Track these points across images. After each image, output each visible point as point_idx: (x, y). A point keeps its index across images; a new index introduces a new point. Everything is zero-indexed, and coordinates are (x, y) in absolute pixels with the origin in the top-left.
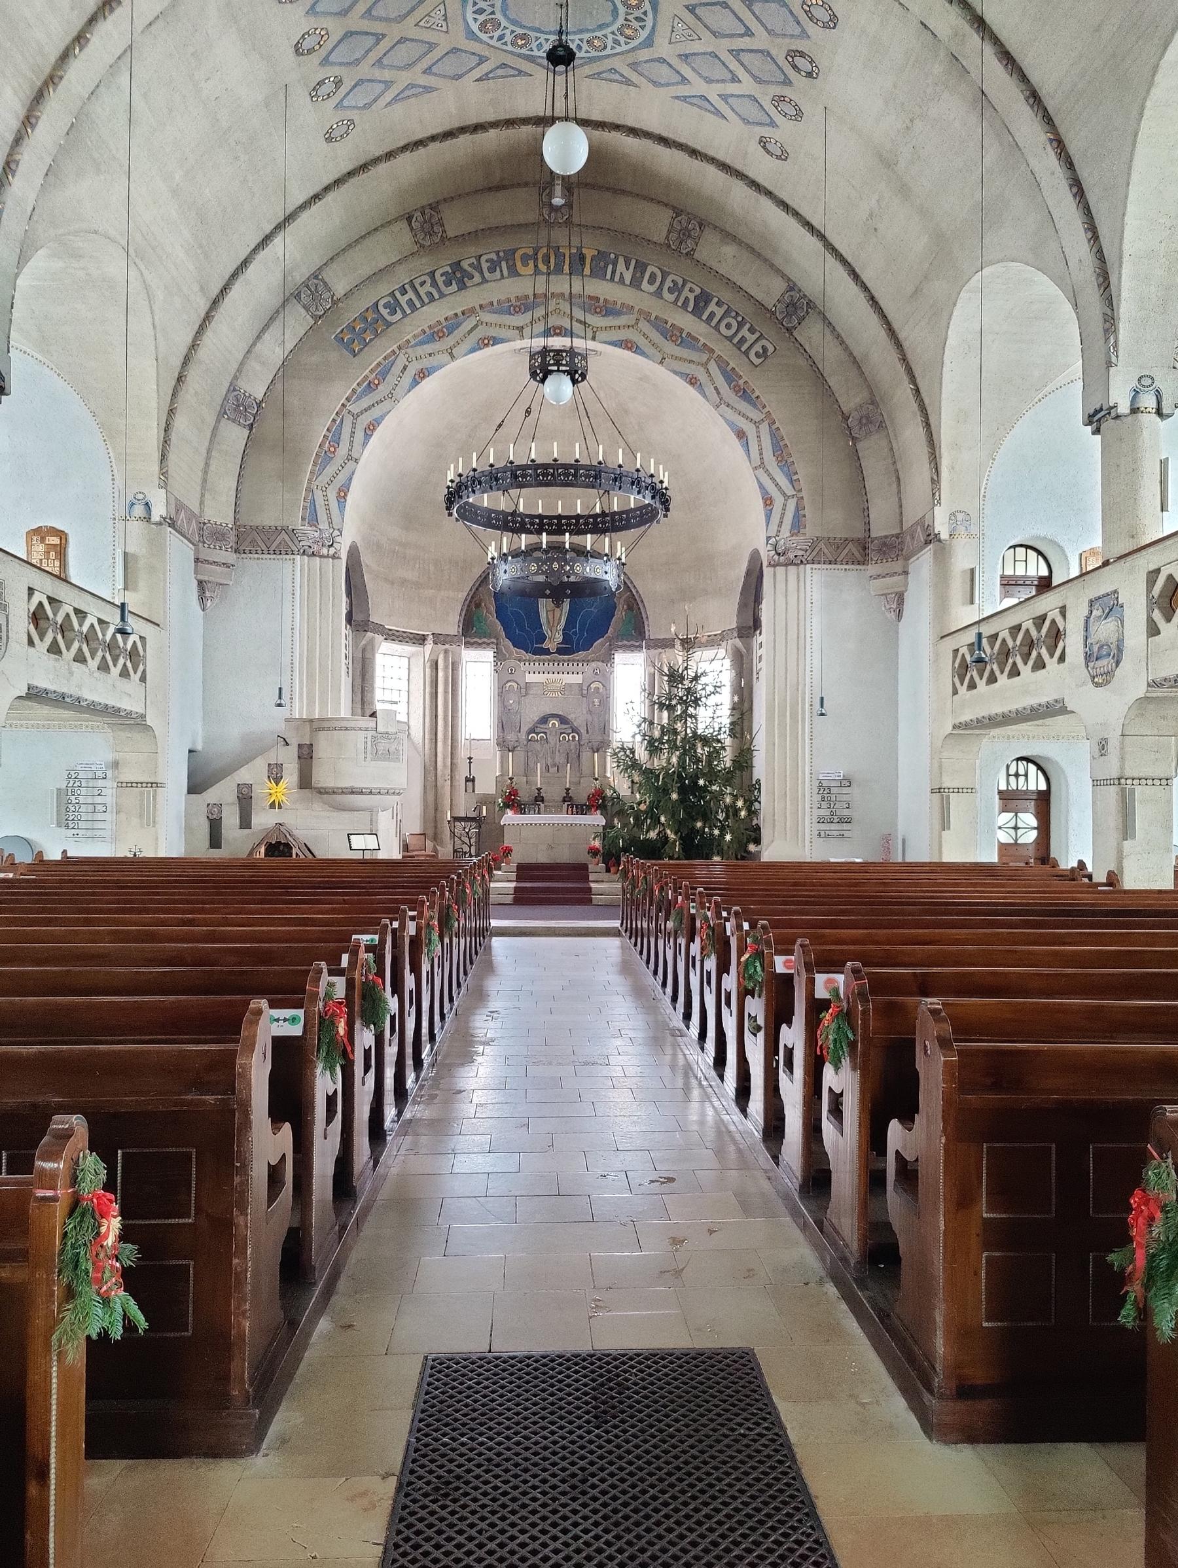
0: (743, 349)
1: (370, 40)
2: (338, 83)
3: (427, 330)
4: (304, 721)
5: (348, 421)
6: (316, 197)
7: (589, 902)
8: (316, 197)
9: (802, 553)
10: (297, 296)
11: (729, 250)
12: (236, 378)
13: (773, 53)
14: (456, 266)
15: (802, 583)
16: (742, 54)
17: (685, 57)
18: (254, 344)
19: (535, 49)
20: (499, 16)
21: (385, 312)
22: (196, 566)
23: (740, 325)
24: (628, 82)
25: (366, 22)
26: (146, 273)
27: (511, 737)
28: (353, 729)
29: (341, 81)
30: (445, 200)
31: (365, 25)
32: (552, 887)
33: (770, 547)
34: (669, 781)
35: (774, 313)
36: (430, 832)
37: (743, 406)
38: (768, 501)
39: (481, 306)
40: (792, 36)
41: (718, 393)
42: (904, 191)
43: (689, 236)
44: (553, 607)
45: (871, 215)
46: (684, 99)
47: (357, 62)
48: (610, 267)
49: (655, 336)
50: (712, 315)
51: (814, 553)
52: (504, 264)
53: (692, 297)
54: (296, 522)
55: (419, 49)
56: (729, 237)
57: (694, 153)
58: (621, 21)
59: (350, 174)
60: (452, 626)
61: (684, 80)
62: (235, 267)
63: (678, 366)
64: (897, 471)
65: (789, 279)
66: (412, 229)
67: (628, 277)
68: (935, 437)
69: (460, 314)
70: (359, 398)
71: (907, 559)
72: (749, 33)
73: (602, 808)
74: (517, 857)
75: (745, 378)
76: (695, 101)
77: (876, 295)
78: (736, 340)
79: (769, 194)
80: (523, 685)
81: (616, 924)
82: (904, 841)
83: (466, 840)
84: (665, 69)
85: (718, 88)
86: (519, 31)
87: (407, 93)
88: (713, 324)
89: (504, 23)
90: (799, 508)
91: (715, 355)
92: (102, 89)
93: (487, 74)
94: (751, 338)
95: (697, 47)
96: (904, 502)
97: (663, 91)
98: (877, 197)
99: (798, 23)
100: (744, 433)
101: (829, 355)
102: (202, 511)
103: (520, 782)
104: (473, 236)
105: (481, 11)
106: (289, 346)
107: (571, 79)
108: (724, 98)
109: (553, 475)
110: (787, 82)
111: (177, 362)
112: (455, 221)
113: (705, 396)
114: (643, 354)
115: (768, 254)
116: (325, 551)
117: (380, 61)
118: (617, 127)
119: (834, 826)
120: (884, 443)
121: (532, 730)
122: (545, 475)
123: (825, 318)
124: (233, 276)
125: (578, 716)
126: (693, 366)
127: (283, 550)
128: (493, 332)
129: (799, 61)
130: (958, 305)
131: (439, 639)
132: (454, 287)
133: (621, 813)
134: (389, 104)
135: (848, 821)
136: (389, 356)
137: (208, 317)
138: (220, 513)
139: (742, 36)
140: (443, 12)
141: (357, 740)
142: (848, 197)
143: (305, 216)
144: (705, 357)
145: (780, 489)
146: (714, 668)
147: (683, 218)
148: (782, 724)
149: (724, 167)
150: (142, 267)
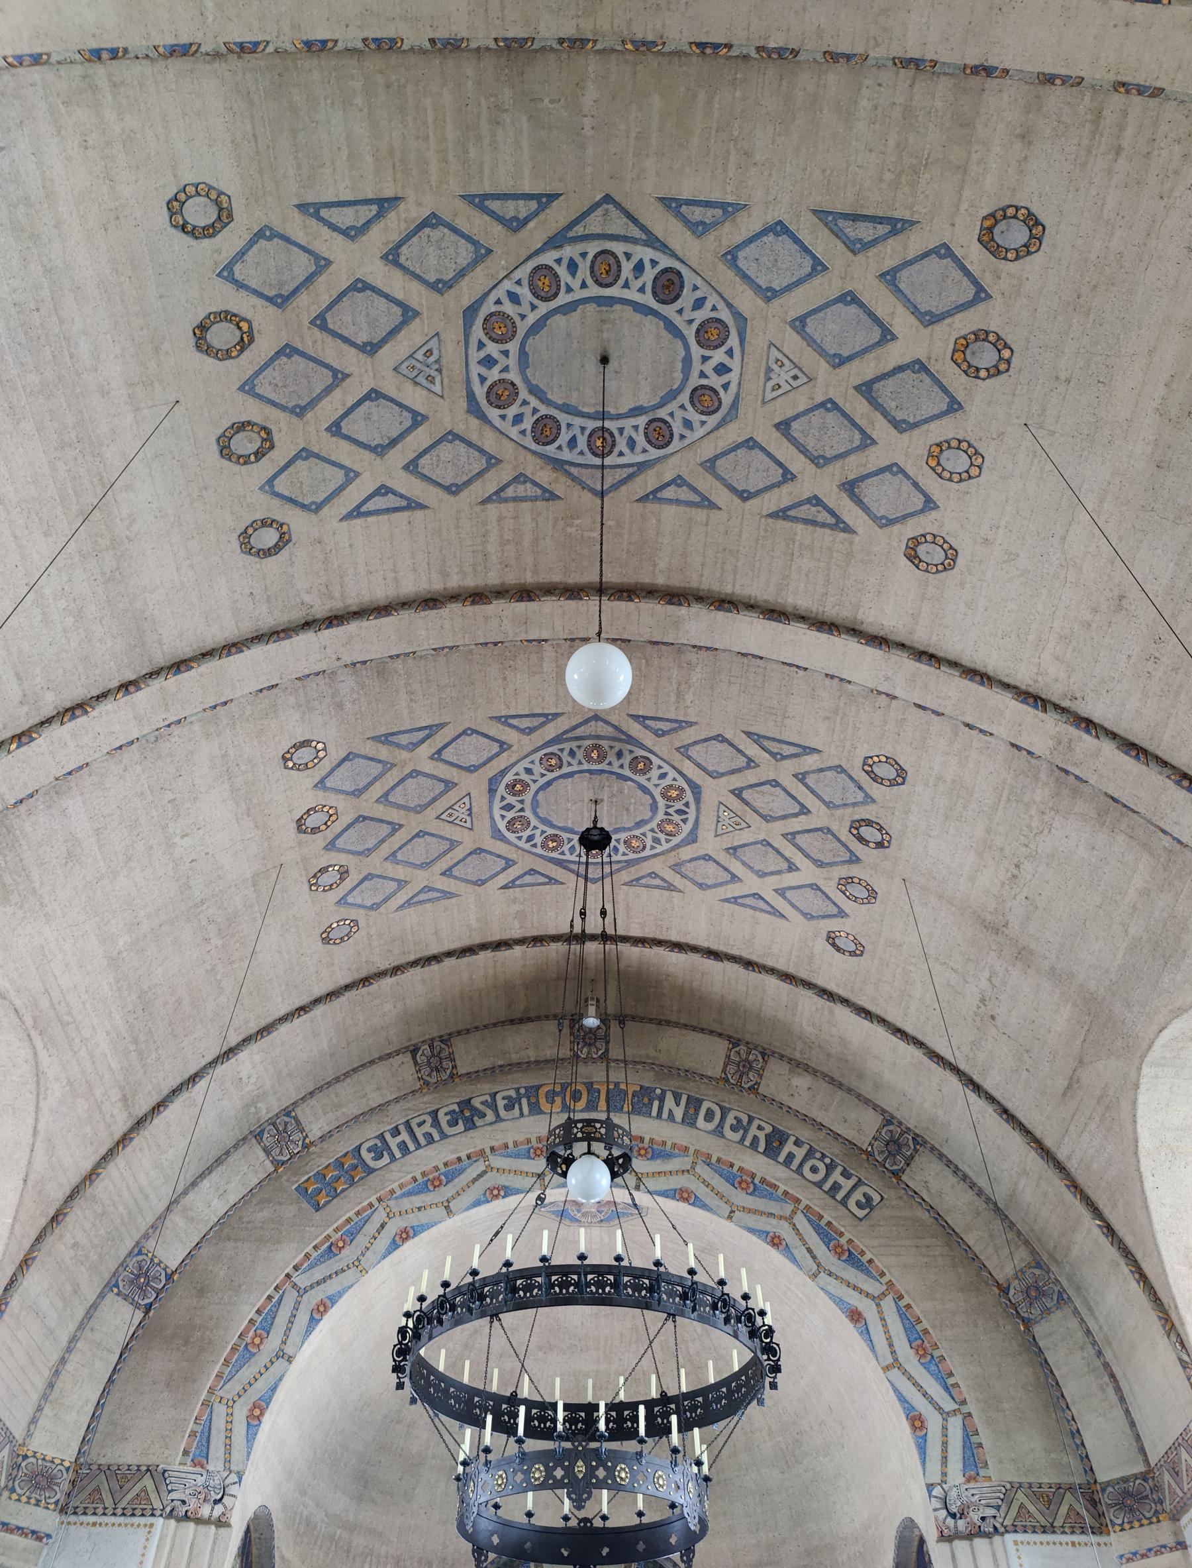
1: (385, 830)
2: (344, 873)
3: (419, 1177)
5: (291, 1297)
6: (303, 1009)
8: (303, 1009)
9: (992, 1512)
10: (259, 1136)
11: (802, 1082)
12: (146, 1236)
13: (834, 827)
14: (466, 1104)
16: (798, 837)
17: (733, 850)
19: (567, 852)
20: (528, 813)
23: (830, 1168)
24: (670, 887)
25: (381, 807)
26: (42, 1054)
29: (347, 872)
30: (459, 1033)
31: (380, 811)
33: (937, 1504)
35: (869, 1154)
37: (851, 1274)
38: (917, 1422)
39: (492, 1149)
40: (854, 804)
41: (814, 1257)
42: (1023, 955)
43: (751, 1068)
45: (983, 1000)
46: (735, 900)
47: (367, 852)
48: (656, 1104)
49: (718, 1182)
50: (791, 1156)
51: (1013, 1512)
52: (524, 1101)
53: (761, 1136)
54: (175, 1463)
55: (436, 847)
56: (800, 1066)
57: (749, 964)
58: (661, 815)
59: (348, 987)
61: (734, 878)
62: (179, 1081)
63: (751, 1220)
64: (1106, 1365)
65: (883, 1111)
66: (416, 1063)
67: (679, 1113)
68: (1162, 1295)
69: (464, 1157)
70: (311, 1267)
71: (1175, 1518)
72: (804, 810)
75: (848, 1236)
76: (748, 901)
77: (1009, 1106)
78: (827, 1187)
79: (845, 1002)
84: (711, 868)
85: (774, 881)
86: (550, 831)
87: (422, 897)
89: (534, 822)
90: (969, 1433)
91: (801, 1206)
92: (38, 802)
93: (513, 881)
94: (847, 1184)
95: (746, 837)
96: (1136, 1416)
97: (709, 893)
98: (986, 974)
99: (860, 788)
100: (860, 1314)
101: (956, 1202)
102: (29, 1434)
104: (491, 1072)
105: (509, 807)
106: (233, 1198)
107: (608, 887)
108: (781, 892)
109: (577, 1285)
110: (854, 860)
111: (58, 1194)
112: (468, 1056)
113: (794, 1260)
114: (704, 1206)
115: (851, 1081)
116: (205, 1511)
117: (394, 854)
118: (659, 943)
120: (1073, 1323)
122: (564, 1285)
123: (941, 1156)
124: (174, 1092)
126: (774, 1221)
127: (140, 1509)
128: (504, 1180)
129: (866, 832)
130: (1143, 1087)
134: (401, 907)
136: (364, 1209)
137: (124, 1140)
138: (57, 1442)
139: (796, 815)
140: (468, 807)
142: (949, 985)
143: (284, 1028)
144: (788, 1208)
145: (931, 1401)
147: (742, 1048)
149: (787, 977)
150: (39, 1044)
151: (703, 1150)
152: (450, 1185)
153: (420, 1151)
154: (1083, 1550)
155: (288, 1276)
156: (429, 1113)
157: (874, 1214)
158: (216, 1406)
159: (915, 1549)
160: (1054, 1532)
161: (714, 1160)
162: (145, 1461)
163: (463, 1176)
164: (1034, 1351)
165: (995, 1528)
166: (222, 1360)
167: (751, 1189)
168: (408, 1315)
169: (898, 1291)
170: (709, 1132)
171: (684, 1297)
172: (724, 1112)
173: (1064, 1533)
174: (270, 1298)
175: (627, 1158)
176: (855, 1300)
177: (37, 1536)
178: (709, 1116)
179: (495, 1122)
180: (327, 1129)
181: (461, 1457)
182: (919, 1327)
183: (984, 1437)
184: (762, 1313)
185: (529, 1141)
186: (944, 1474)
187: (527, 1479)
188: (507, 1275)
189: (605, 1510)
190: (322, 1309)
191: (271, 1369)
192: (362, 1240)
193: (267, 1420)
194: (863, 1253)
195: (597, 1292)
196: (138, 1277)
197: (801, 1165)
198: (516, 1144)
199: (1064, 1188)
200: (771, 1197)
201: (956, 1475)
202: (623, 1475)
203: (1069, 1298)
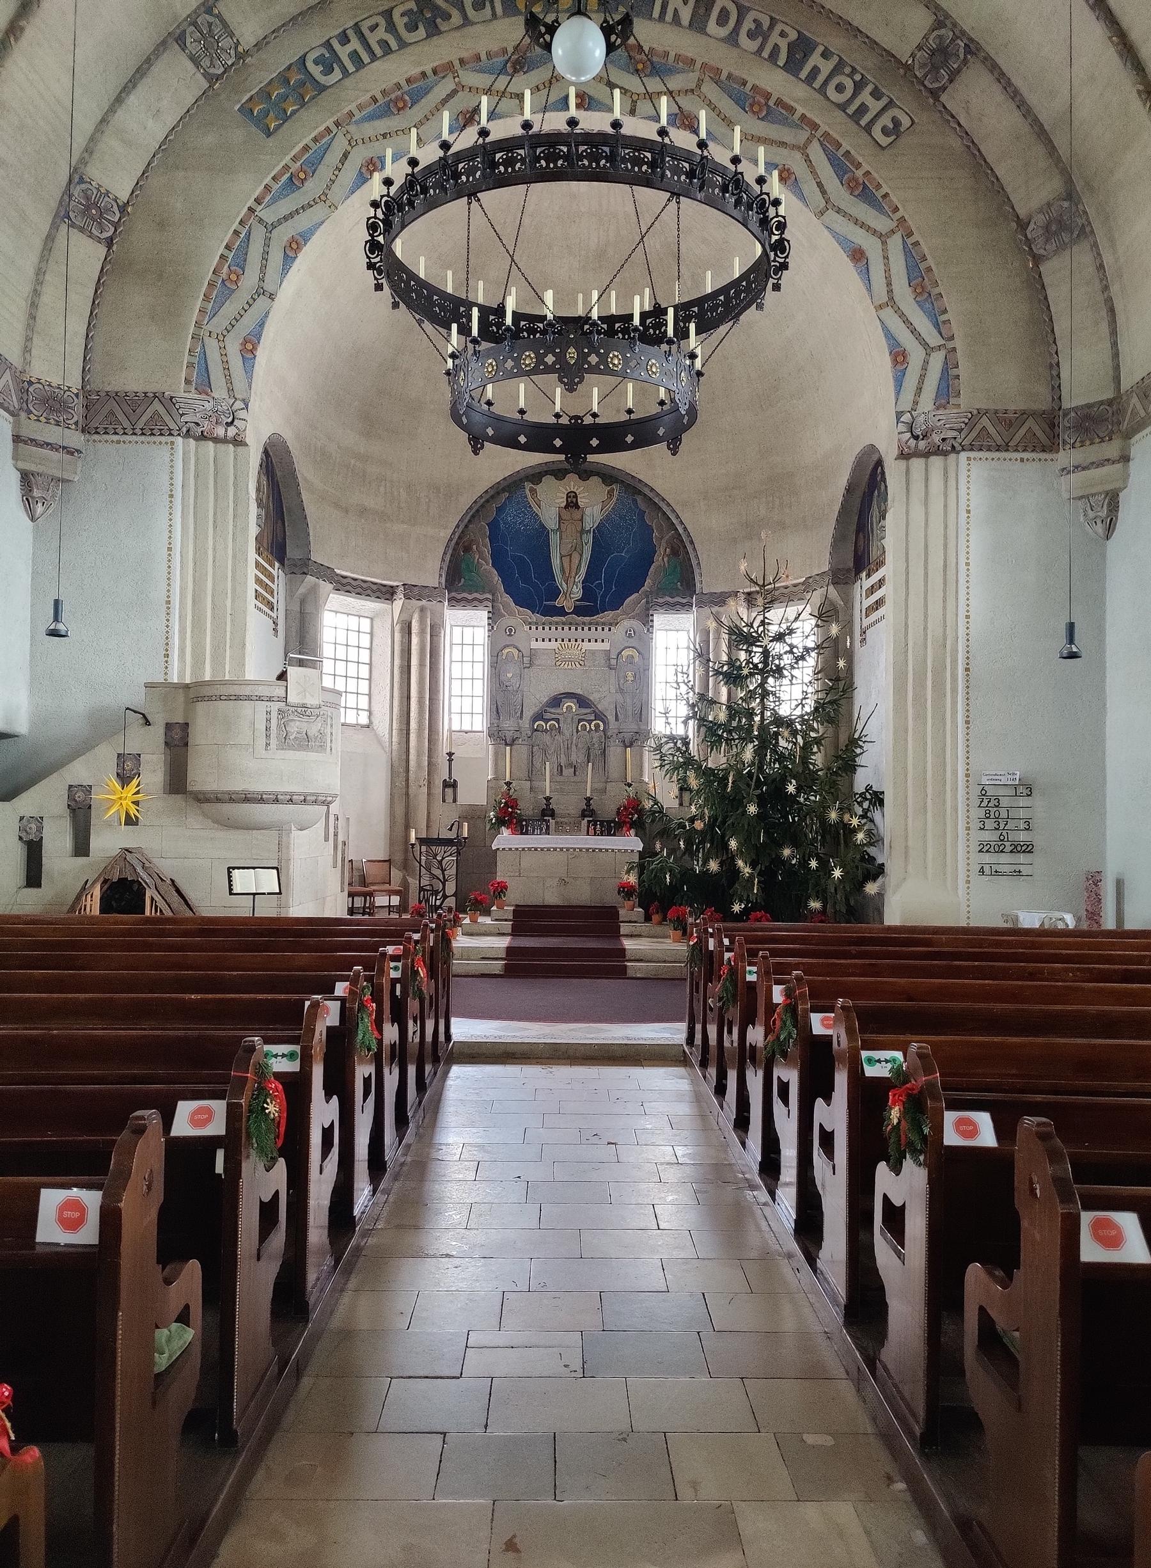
0: (863, 123)
3: (379, 96)
4: (176, 687)
5: (258, 234)
7: (620, 972)
9: (955, 434)
15: (952, 483)
18: (112, 110)
21: (316, 70)
22: (15, 450)
23: (859, 87)
27: (509, 725)
28: (249, 698)
32: (565, 949)
33: (902, 427)
34: (743, 786)
35: (908, 68)
36: (398, 857)
37: (862, 211)
38: (899, 357)
39: (462, 61)
41: (823, 192)
44: (566, 536)
50: (815, 71)
51: (974, 434)
53: (783, 45)
54: (180, 391)
60: (432, 574)
67: (686, 15)
69: (429, 73)
70: (274, 200)
71: (1128, 436)
73: (639, 827)
74: (516, 895)
75: (866, 167)
78: (851, 110)
80: (526, 652)
81: (672, 1033)
82: (1120, 884)
83: (438, 872)
88: (817, 84)
91: (819, 134)
94: (874, 106)
103: (521, 788)
106: (171, 120)
109: (566, 157)
116: (220, 431)
119: (1004, 858)
121: (538, 716)
122: (551, 157)
125: (604, 696)
126: (785, 152)
127: (155, 429)
131: (412, 592)
132: (421, 32)
133: (666, 834)
135: (1028, 849)
138: (57, 366)
141: (254, 715)
144: (803, 136)
146: (798, 625)
148: (919, 700)
151: (712, 63)
152: (416, 108)
153: (376, 63)
154: (1028, 465)
155: (251, 210)
156: (381, 14)
157: (903, 140)
158: (206, 339)
159: (869, 472)
160: (1007, 450)
161: (724, 76)
162: (151, 388)
163: (430, 96)
164: (1037, 288)
165: (953, 447)
166: (202, 296)
167: (764, 113)
168: (375, 204)
169: (909, 227)
170: (722, 40)
171: (691, 175)
172: (742, 11)
173: (1016, 450)
174: (236, 233)
175: (627, 21)
176: (860, 238)
177: (70, 452)
178: (723, 19)
179: (463, 26)
180: (261, 34)
181: (450, 350)
182: (922, 266)
183: (964, 370)
184: (776, 203)
185: (504, 51)
186: (916, 403)
187: (517, 364)
188: (484, 146)
189: (595, 409)
190: (294, 247)
191: (255, 306)
192: (324, 172)
193: (262, 354)
194: (879, 186)
195: (590, 165)
196: (88, 208)
197: (826, 83)
198: (489, 55)
199: (1135, 94)
200: (784, 122)
201: (927, 402)
202: (616, 362)
203: (1092, 232)
